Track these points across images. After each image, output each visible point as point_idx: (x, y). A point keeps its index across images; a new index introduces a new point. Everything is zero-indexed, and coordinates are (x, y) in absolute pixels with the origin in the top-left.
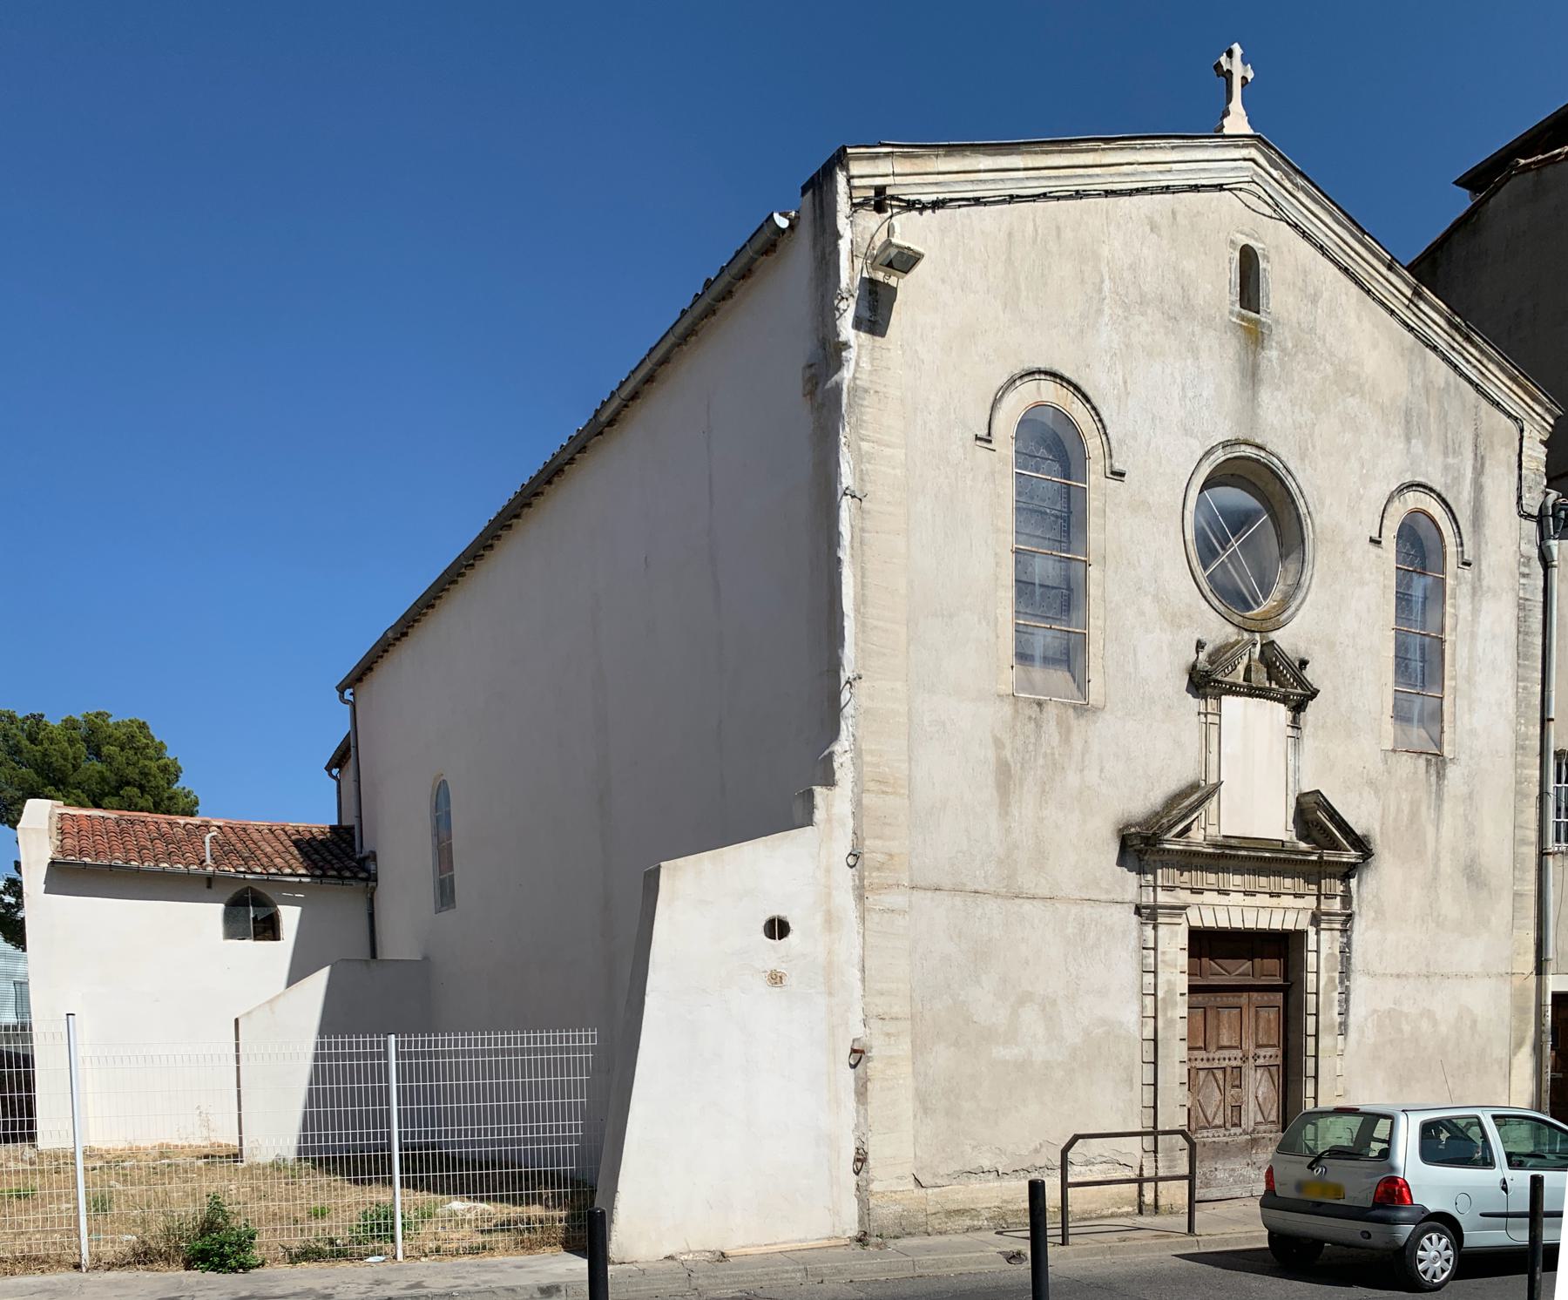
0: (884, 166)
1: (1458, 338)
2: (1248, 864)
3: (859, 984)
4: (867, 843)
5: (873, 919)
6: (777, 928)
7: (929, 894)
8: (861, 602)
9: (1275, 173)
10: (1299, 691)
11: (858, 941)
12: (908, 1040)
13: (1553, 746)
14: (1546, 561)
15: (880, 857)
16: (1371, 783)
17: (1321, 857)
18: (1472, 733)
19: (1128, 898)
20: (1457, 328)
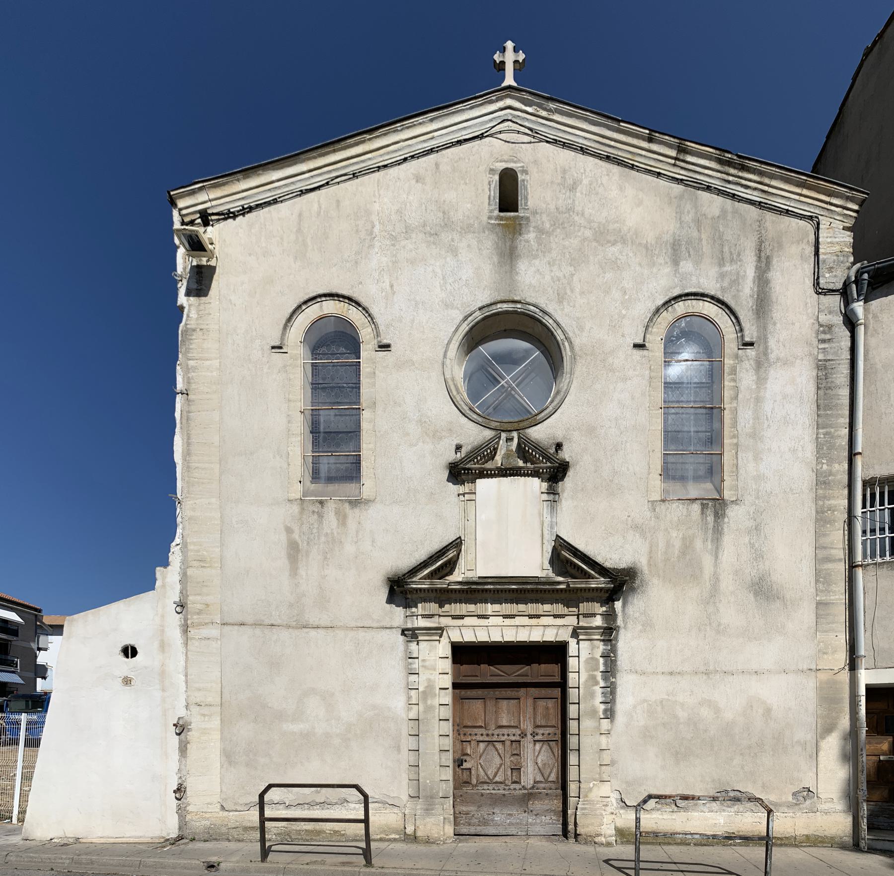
0: (202, 197)
1: (732, 171)
2: (504, 595)
3: (184, 684)
4: (190, 598)
5: (194, 645)
6: (130, 652)
7: (236, 627)
8: (187, 454)
9: (529, 109)
10: (549, 464)
11: (182, 658)
12: (219, 718)
13: (860, 474)
14: (851, 323)
15: (199, 606)
16: (636, 527)
17: (568, 585)
18: (759, 478)
19: (395, 624)
20: (729, 163)
